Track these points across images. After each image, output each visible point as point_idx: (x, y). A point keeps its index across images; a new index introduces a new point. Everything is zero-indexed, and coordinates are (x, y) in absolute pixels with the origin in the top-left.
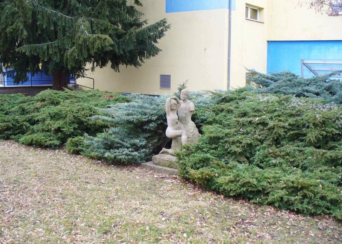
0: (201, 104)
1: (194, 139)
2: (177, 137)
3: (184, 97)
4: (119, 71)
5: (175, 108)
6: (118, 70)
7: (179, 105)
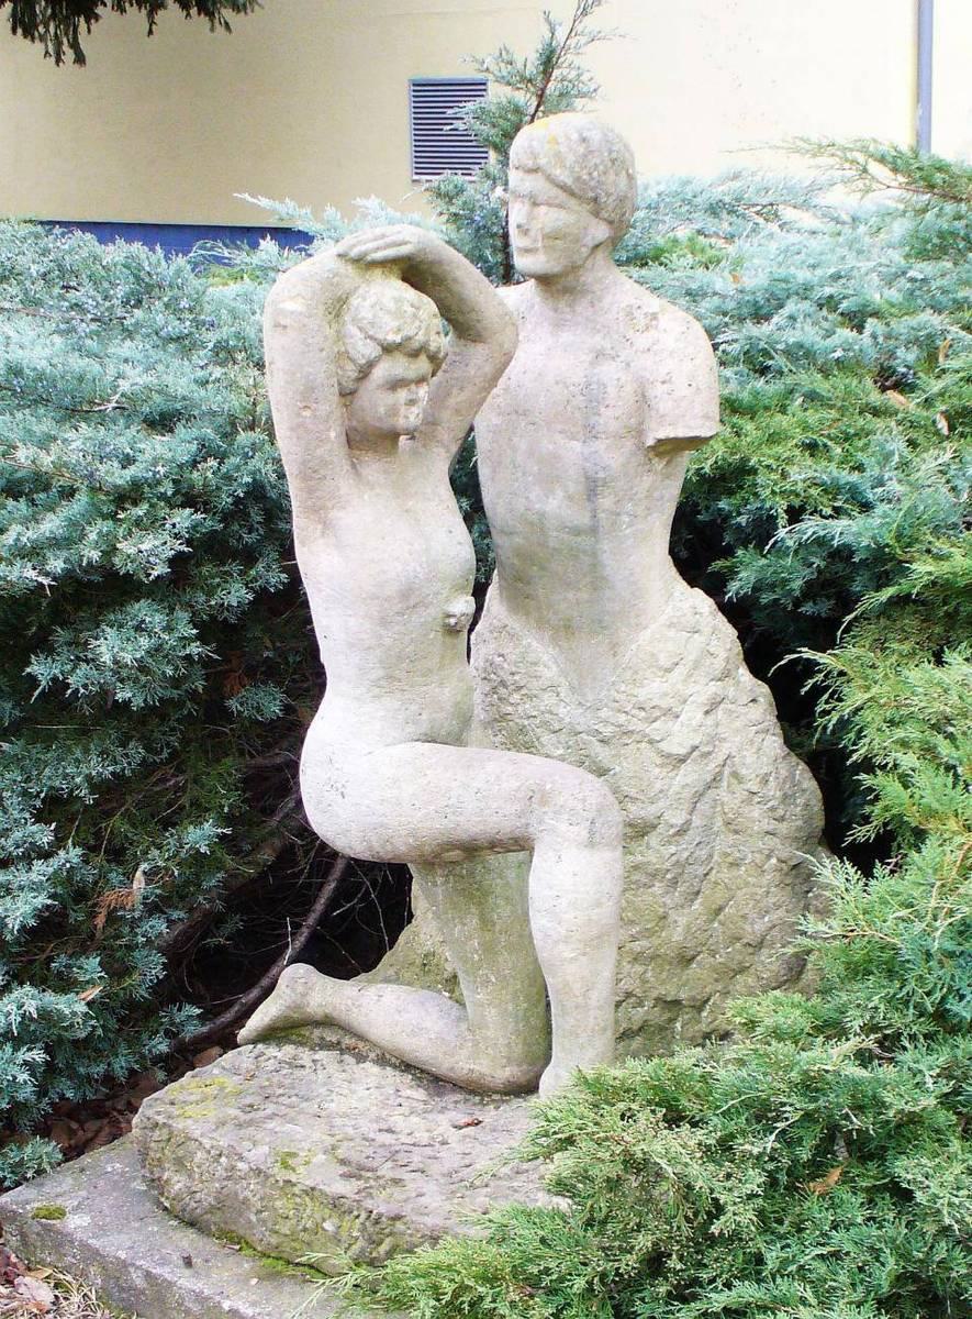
0: (795, 328)
1: (723, 843)
2: (481, 861)
3: (553, 236)
4: (80, 59)
5: (412, 417)
6: (75, 45)
7: (479, 356)
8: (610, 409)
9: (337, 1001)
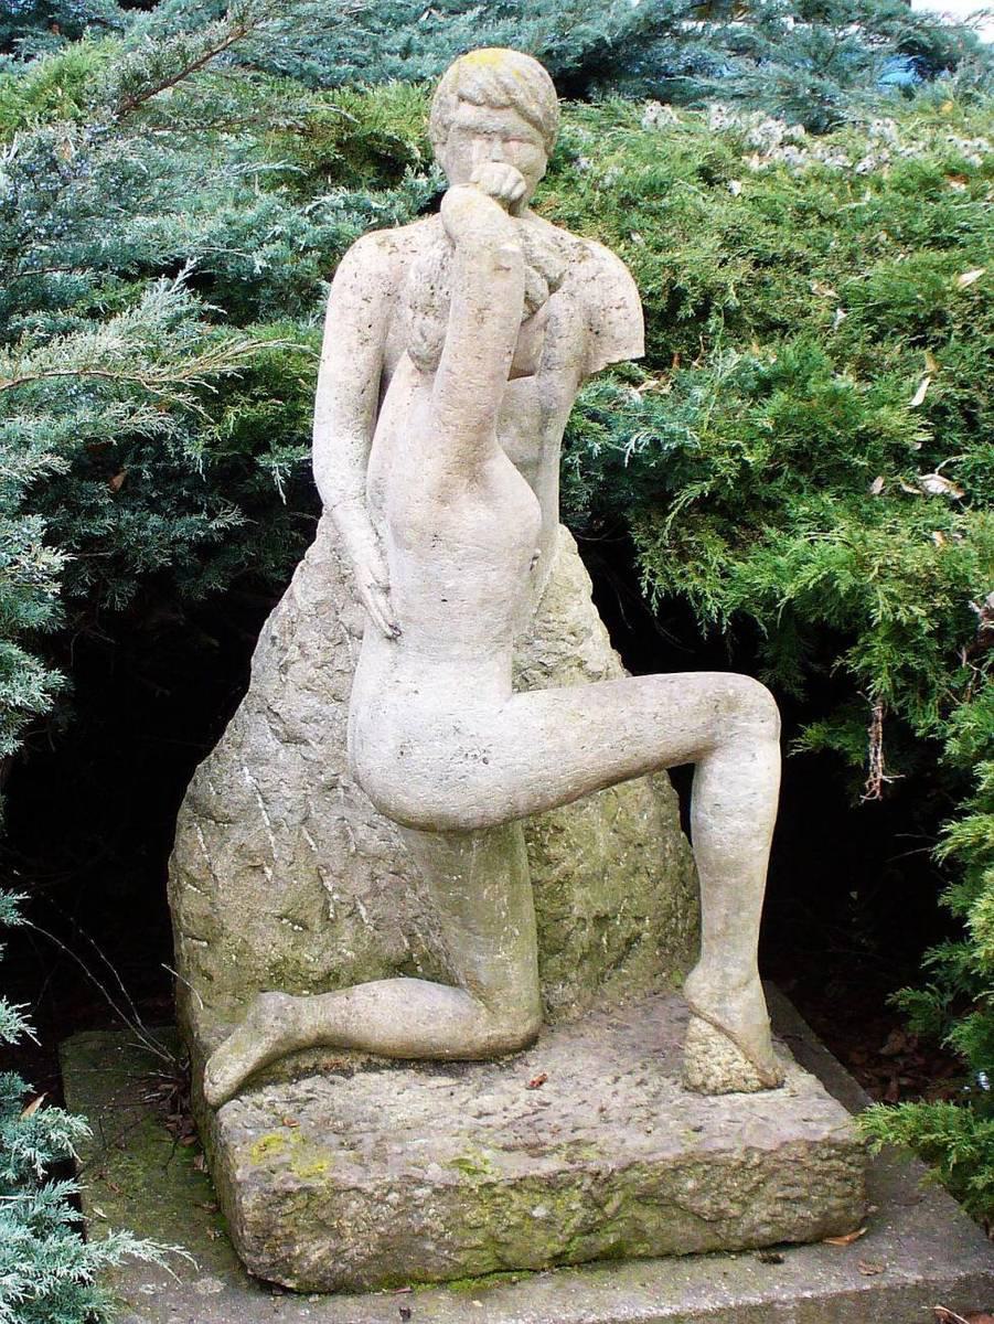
8: (564, 340)
9: (330, 1016)
